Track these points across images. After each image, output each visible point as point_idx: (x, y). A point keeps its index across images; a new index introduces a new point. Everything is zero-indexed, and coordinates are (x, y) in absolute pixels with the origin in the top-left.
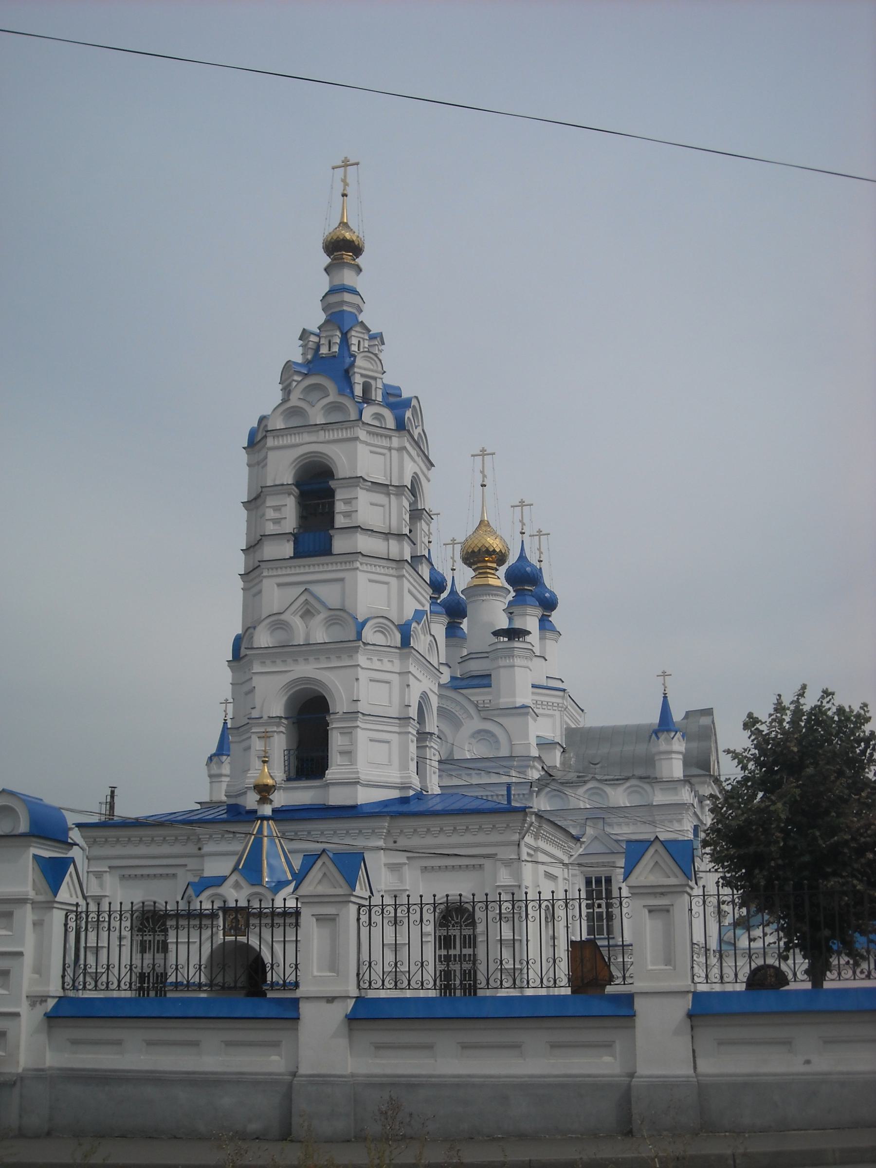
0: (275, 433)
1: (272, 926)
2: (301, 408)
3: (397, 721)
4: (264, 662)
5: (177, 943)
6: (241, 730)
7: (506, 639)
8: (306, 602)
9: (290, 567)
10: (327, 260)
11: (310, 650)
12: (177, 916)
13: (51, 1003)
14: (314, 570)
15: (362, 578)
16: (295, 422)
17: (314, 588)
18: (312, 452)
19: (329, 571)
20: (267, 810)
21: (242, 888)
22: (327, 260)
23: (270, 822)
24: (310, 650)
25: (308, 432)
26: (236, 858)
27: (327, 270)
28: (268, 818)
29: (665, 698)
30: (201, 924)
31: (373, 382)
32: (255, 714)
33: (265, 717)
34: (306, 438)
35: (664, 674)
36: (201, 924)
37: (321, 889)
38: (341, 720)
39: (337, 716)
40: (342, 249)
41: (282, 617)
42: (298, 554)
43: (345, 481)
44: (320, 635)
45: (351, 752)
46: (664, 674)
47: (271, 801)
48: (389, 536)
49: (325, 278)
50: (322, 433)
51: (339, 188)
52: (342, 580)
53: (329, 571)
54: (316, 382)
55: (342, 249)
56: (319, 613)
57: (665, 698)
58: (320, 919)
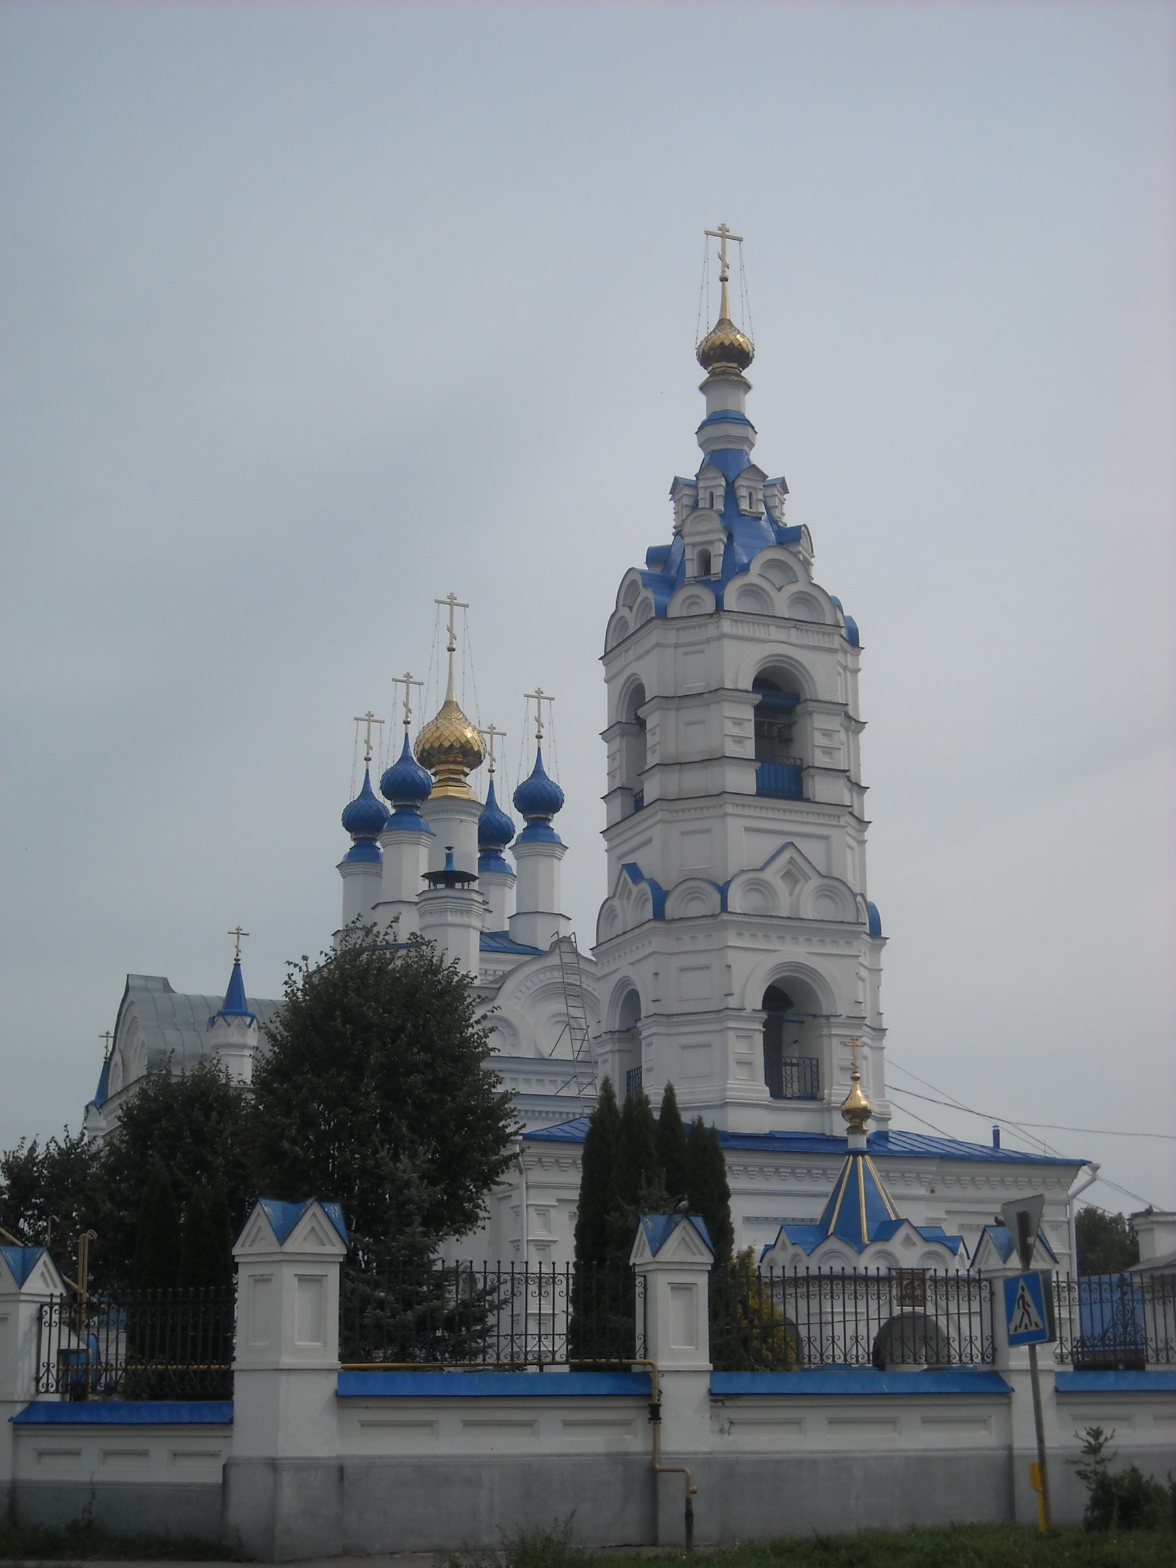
0: (732, 616)
1: (808, 1297)
2: (762, 589)
3: (871, 1031)
4: (768, 936)
5: (832, 1313)
6: (675, 1019)
7: (443, 886)
8: (791, 861)
9: (743, 806)
10: (703, 375)
11: (795, 925)
12: (785, 1282)
13: (19, 1409)
14: (782, 817)
15: (735, 826)
16: (801, 614)
17: (798, 842)
18: (795, 660)
19: (814, 824)
20: (861, 1142)
21: (914, 1244)
22: (703, 375)
23: (867, 1157)
24: (795, 925)
25: (777, 626)
26: (824, 1202)
27: (703, 388)
28: (863, 1153)
29: (237, 966)
30: (808, 1292)
31: (709, 548)
32: (733, 1002)
33: (749, 1009)
34: (774, 633)
35: (238, 932)
36: (808, 1292)
37: (312, 1247)
38: (843, 1025)
39: (839, 1020)
40: (725, 359)
41: (762, 875)
42: (762, 792)
43: (829, 706)
44: (809, 909)
45: (750, 1063)
46: (238, 932)
47: (864, 1132)
48: (855, 787)
49: (702, 399)
50: (793, 631)
51: (716, 270)
52: (826, 838)
53: (814, 824)
54: (776, 557)
55: (725, 359)
56: (807, 878)
57: (237, 966)
58: (676, 1287)
